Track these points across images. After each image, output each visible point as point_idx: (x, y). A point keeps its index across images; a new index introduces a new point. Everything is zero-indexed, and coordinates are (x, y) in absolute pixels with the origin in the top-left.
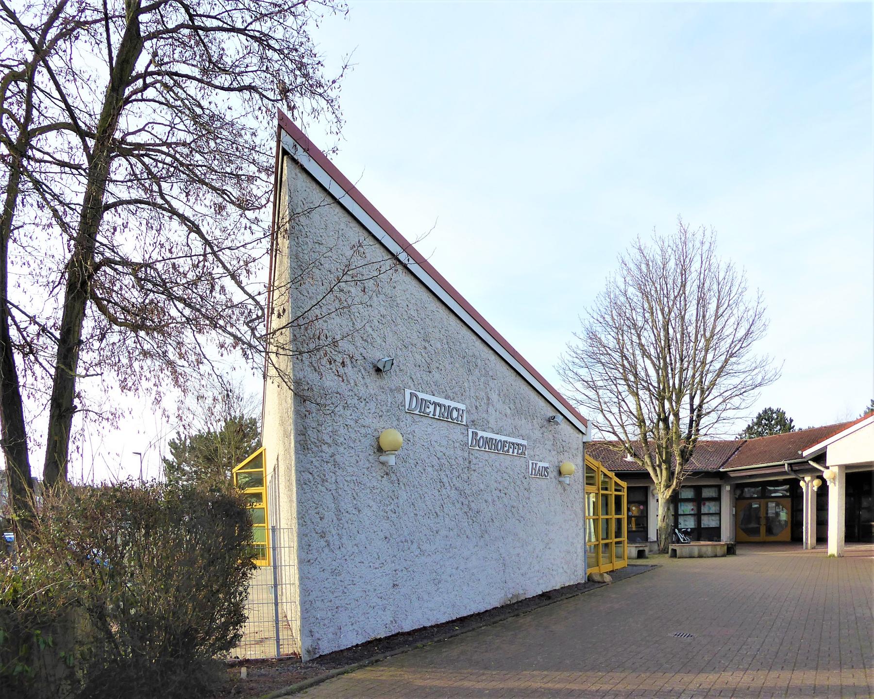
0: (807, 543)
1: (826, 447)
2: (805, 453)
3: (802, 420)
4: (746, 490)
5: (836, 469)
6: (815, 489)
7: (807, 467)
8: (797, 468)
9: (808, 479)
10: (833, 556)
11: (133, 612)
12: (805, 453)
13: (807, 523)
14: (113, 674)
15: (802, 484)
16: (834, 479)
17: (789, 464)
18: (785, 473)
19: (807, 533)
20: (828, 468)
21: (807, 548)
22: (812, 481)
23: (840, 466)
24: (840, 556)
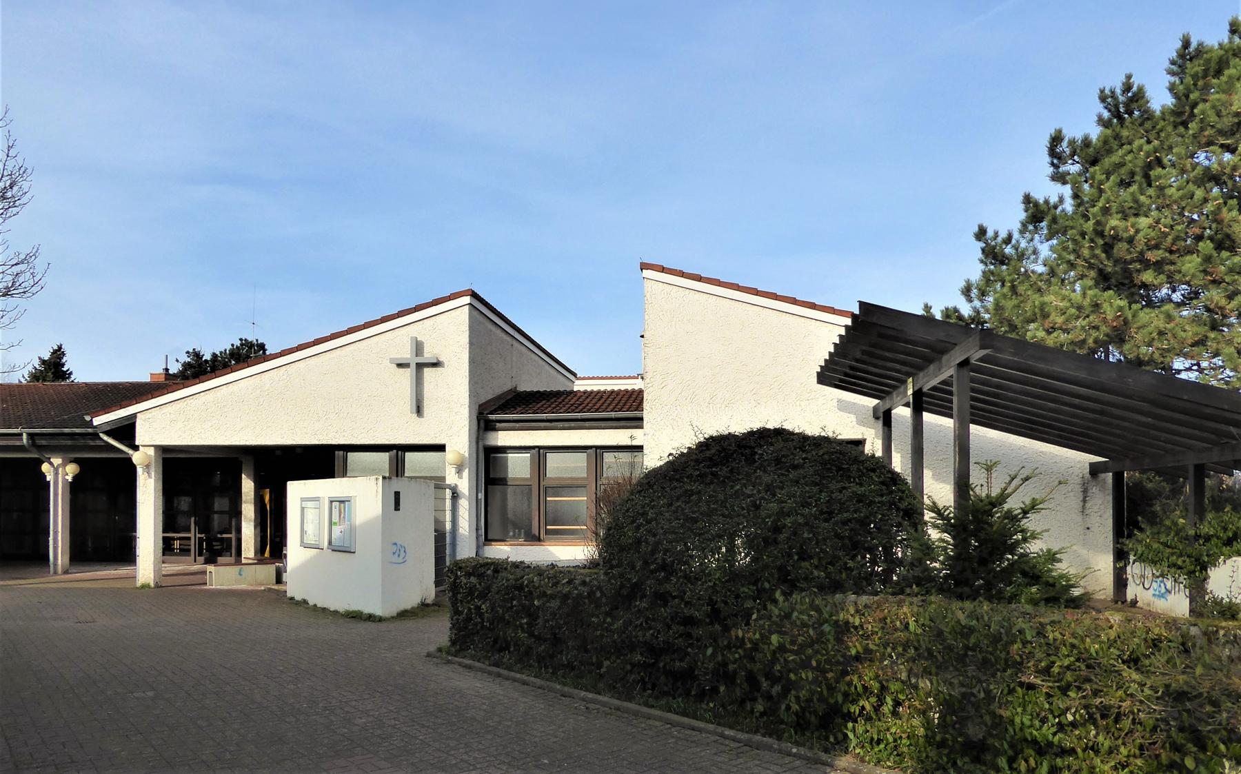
0: (55, 565)
1: (134, 416)
2: (97, 421)
3: (85, 369)
4: (296, 490)
5: (151, 451)
6: (69, 478)
7: (98, 443)
8: (44, 443)
9: (57, 461)
10: (148, 586)
11: (709, 651)
12: (97, 421)
13: (56, 533)
14: (1019, 710)
15: (45, 467)
16: (148, 466)
17: (29, 435)
18: (21, 449)
19: (55, 548)
20: (136, 448)
21: (55, 573)
22: (64, 465)
23: (157, 447)
24: (157, 586)
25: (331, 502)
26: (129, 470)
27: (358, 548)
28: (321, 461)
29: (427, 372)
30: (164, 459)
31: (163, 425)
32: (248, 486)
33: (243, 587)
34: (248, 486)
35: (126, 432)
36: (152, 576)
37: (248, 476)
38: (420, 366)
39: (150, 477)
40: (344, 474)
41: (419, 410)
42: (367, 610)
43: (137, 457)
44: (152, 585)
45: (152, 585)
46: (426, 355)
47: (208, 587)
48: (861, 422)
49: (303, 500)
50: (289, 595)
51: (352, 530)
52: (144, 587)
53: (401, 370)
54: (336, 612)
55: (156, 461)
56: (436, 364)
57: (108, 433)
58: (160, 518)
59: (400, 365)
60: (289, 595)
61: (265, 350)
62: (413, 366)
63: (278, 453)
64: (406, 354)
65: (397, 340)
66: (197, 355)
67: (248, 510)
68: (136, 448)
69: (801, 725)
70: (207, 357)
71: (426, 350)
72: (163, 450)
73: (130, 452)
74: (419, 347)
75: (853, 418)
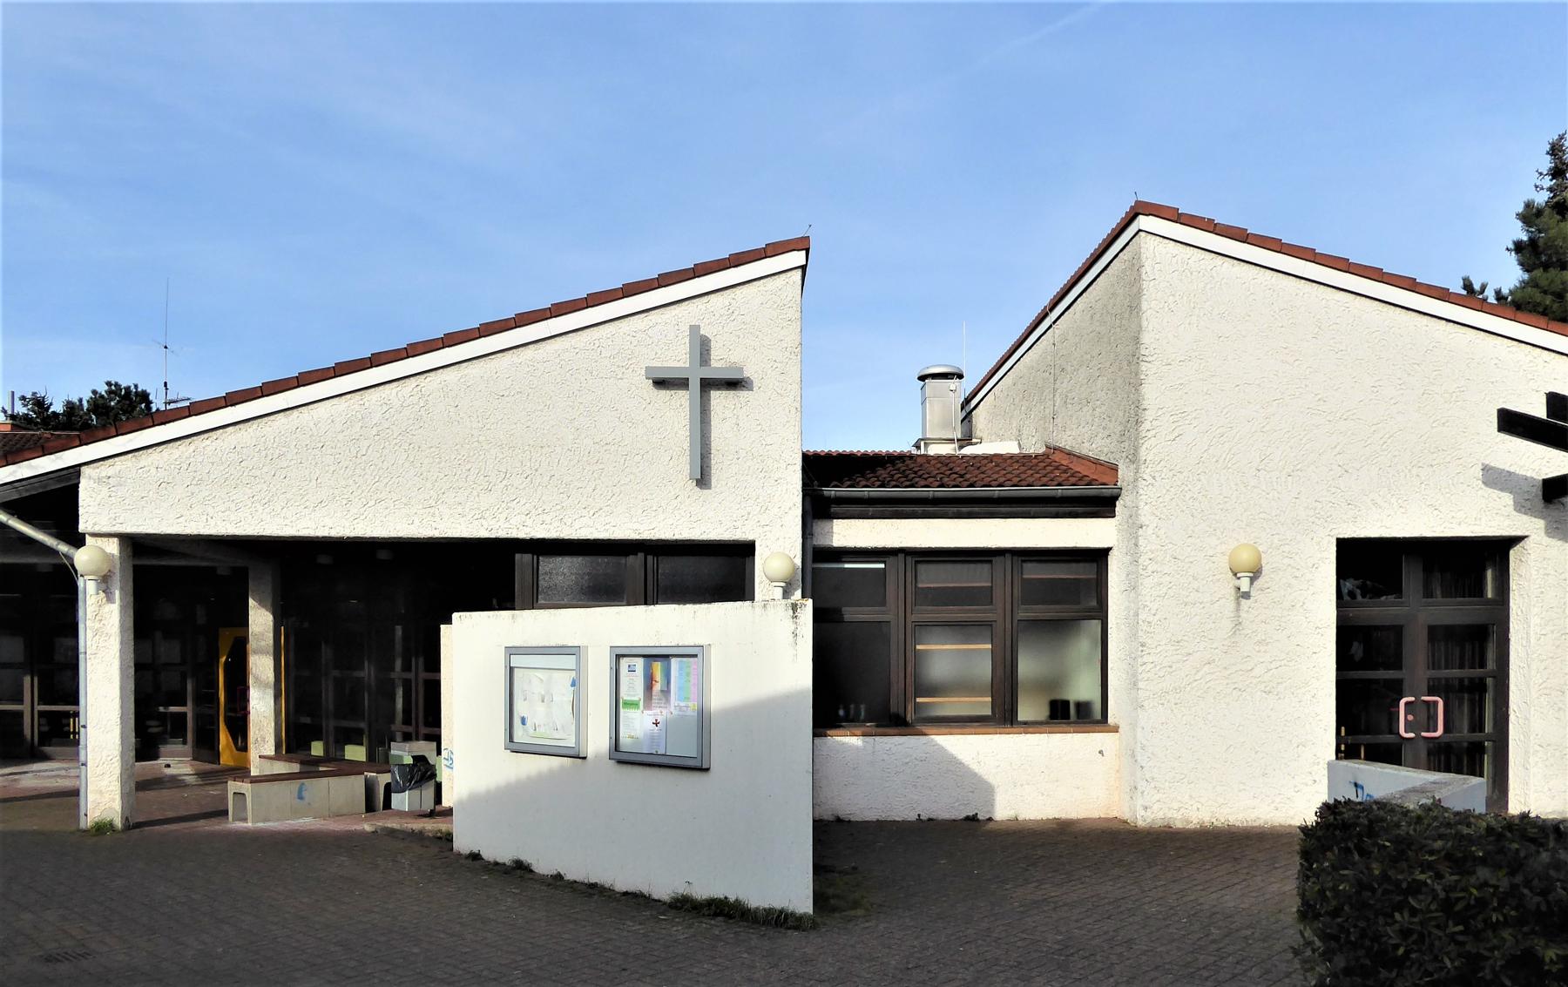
1: (74, 472)
5: (113, 547)
24: (130, 826)
25: (618, 657)
26: (64, 582)
27: (716, 761)
28: (489, 572)
29: (718, 398)
30: (135, 567)
31: (129, 494)
32: (260, 621)
33: (306, 823)
34: (260, 621)
35: (56, 504)
36: (117, 805)
37: (261, 603)
38: (708, 385)
39: (110, 599)
40: (532, 604)
41: (703, 480)
42: (757, 899)
43: (82, 558)
44: (118, 823)
45: (118, 823)
46: (714, 364)
47: (234, 825)
48: (1520, 507)
49: (511, 651)
50: (462, 844)
51: (703, 719)
52: (102, 828)
53: (664, 394)
54: (637, 900)
55: (122, 569)
56: (734, 384)
57: (12, 507)
58: (132, 686)
59: (661, 383)
60: (462, 844)
61: (149, 403)
62: (695, 385)
63: (383, 555)
64: (678, 358)
65: (661, 333)
66: (39, 404)
67: (262, 667)
68: (78, 541)
69: (45, 739)
70: (58, 407)
71: (714, 354)
72: (135, 545)
73: (63, 548)
74: (703, 348)
75: (1507, 499)
